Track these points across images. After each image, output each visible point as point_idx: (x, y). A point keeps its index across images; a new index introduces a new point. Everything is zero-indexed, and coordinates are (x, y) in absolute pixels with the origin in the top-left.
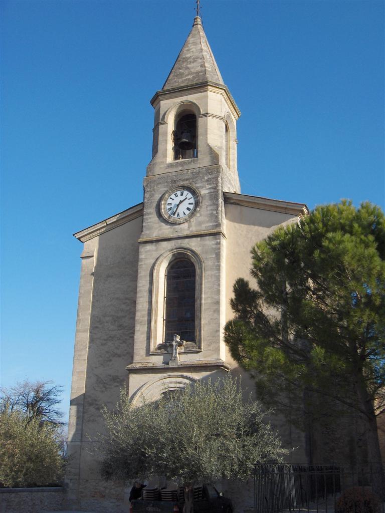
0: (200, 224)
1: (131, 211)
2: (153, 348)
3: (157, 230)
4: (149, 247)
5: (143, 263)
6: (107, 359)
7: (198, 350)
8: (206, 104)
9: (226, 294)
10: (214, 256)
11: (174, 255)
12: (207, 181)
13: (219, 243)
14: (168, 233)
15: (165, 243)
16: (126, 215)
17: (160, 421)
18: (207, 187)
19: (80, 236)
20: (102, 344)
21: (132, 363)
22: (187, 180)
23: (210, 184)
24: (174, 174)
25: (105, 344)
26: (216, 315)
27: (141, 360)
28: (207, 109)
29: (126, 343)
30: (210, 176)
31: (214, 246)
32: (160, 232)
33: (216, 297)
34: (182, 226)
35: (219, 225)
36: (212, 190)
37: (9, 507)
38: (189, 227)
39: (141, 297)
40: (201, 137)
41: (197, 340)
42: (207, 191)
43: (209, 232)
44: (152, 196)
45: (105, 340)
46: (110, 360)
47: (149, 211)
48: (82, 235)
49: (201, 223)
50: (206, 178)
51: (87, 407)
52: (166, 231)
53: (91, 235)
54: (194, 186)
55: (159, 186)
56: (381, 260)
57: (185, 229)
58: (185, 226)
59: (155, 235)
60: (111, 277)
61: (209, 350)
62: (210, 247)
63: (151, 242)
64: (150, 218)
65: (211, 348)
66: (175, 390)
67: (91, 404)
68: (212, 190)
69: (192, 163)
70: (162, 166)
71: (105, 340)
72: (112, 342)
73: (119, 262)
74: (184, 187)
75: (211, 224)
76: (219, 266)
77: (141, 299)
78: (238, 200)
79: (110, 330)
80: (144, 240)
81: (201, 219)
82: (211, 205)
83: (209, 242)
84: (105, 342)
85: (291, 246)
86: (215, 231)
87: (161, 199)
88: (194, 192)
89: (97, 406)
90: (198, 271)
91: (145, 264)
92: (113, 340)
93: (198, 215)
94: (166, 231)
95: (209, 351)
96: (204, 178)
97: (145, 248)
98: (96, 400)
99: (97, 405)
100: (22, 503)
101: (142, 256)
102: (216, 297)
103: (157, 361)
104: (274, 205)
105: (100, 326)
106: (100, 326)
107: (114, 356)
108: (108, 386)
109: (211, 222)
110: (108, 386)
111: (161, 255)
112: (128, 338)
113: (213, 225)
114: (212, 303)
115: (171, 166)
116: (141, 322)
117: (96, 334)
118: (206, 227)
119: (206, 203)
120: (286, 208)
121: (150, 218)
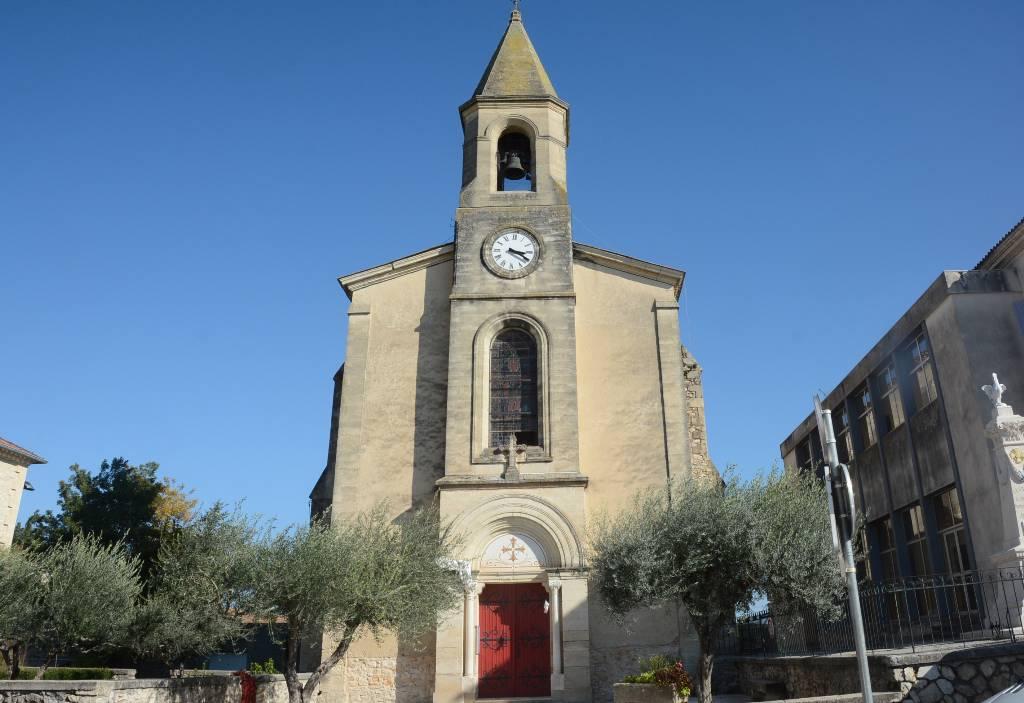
0: (542, 281)
2: (477, 453)
4: (466, 307)
5: (457, 330)
7: (547, 458)
8: (547, 124)
10: (566, 328)
11: (505, 322)
12: (551, 225)
13: (572, 311)
15: (491, 303)
17: (761, 528)
19: (348, 282)
20: (384, 447)
21: (444, 475)
22: (523, 219)
23: (557, 230)
24: (504, 209)
25: (389, 447)
26: (571, 411)
28: (548, 131)
29: (424, 446)
30: (556, 219)
31: (566, 315)
33: (571, 385)
34: (517, 282)
35: (570, 286)
39: (455, 379)
41: (546, 442)
42: (553, 239)
43: (558, 294)
44: (469, 236)
46: (398, 472)
47: (465, 255)
48: (353, 280)
49: (544, 279)
50: (550, 221)
52: (492, 285)
53: (366, 283)
54: (532, 229)
56: (418, 324)
57: (521, 286)
58: (522, 282)
59: (475, 290)
60: (398, 345)
63: (471, 300)
64: (467, 266)
65: (567, 457)
68: (559, 238)
70: (483, 196)
74: (518, 229)
75: (559, 284)
76: (574, 342)
77: (456, 381)
80: (459, 296)
81: (545, 275)
82: (558, 258)
83: (557, 307)
86: (567, 293)
88: (534, 238)
90: (538, 342)
91: (460, 331)
93: (540, 269)
94: (492, 285)
96: (546, 220)
101: (455, 319)
102: (571, 385)
103: (494, 472)
104: (643, 268)
107: (404, 465)
111: (487, 320)
112: (427, 438)
115: (494, 198)
117: (373, 430)
118: (553, 286)
119: (551, 255)
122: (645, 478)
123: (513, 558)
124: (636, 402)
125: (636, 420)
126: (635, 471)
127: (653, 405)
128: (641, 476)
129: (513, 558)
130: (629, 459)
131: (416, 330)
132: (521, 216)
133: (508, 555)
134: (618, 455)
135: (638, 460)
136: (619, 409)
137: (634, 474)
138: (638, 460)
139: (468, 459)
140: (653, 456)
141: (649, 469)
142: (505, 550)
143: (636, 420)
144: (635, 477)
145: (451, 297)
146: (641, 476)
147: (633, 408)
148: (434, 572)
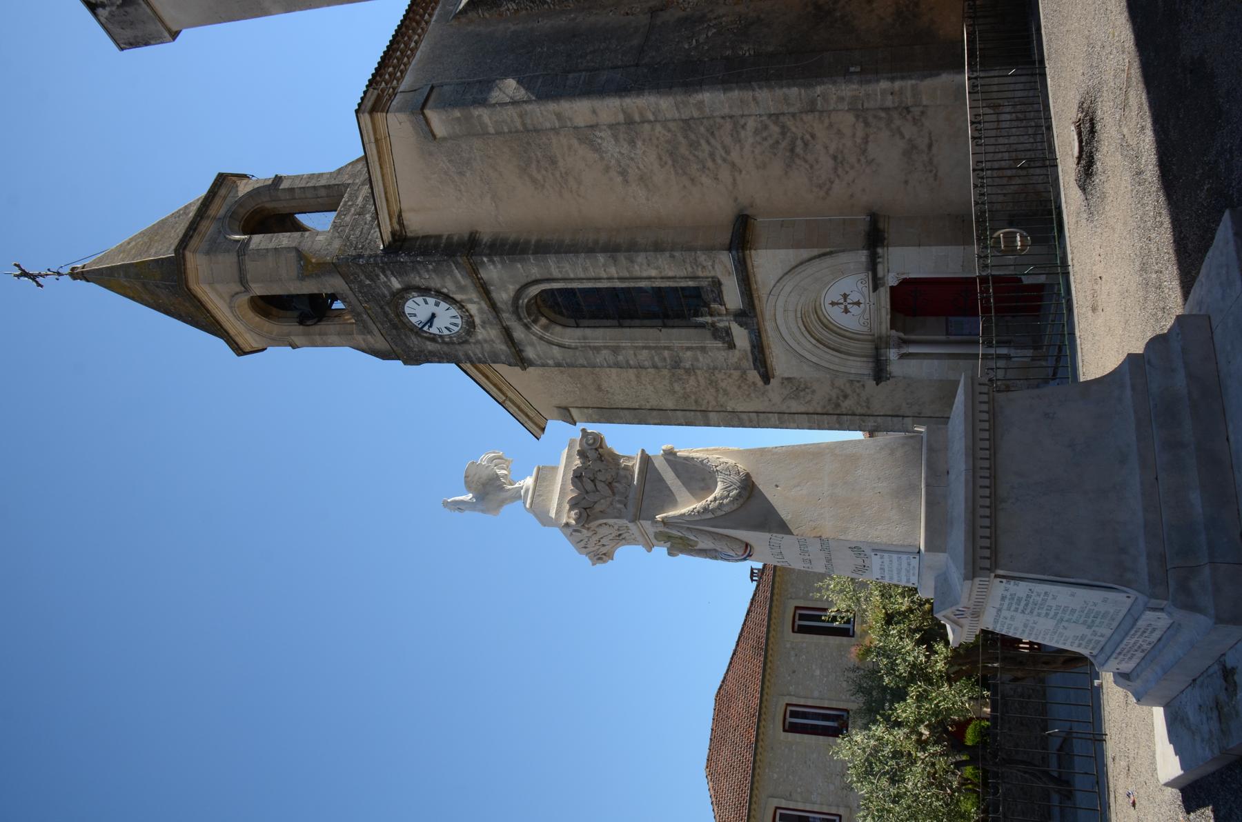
1: (522, 418)
3: (494, 345)
6: (752, 388)
9: (957, 580)
14: (494, 331)
16: (480, 376)
18: (385, 279)
23: (378, 276)
27: (747, 360)
32: (498, 341)
36: (389, 273)
37: (1049, 608)
38: (471, 301)
40: (292, 289)
45: (717, 391)
51: (844, 410)
55: (412, 345)
61: (713, 268)
62: (503, 272)
66: (102, 257)
67: (838, 405)
69: (347, 300)
71: (566, 364)
72: (719, 381)
73: (571, 377)
75: (456, 271)
78: (391, 220)
79: (698, 385)
82: (419, 273)
84: (721, 391)
85: (839, 511)
87: (447, 298)
89: (841, 398)
92: (717, 381)
95: (716, 267)
97: (533, 360)
98: (830, 400)
99: (838, 398)
100: (535, 68)
105: (693, 397)
106: (693, 397)
108: (802, 386)
109: (452, 271)
110: (802, 386)
113: (457, 268)
114: (615, 265)
116: (676, 362)
120: (377, 141)
121: (475, 355)
122: (724, 147)
123: (858, 303)
124: (602, 158)
125: (632, 159)
126: (714, 160)
127: (601, 138)
128: (720, 152)
129: (858, 303)
130: (695, 166)
131: (649, 550)
132: (470, 267)
133: (854, 310)
134: (692, 180)
135: (695, 156)
136: (619, 179)
137: (719, 161)
138: (695, 156)
139: (779, 806)
140: (686, 137)
141: (708, 142)
142: (846, 311)
143: (632, 159)
144: (724, 160)
145: (520, 128)
146: (720, 152)
147: (613, 162)
148: (868, 249)
